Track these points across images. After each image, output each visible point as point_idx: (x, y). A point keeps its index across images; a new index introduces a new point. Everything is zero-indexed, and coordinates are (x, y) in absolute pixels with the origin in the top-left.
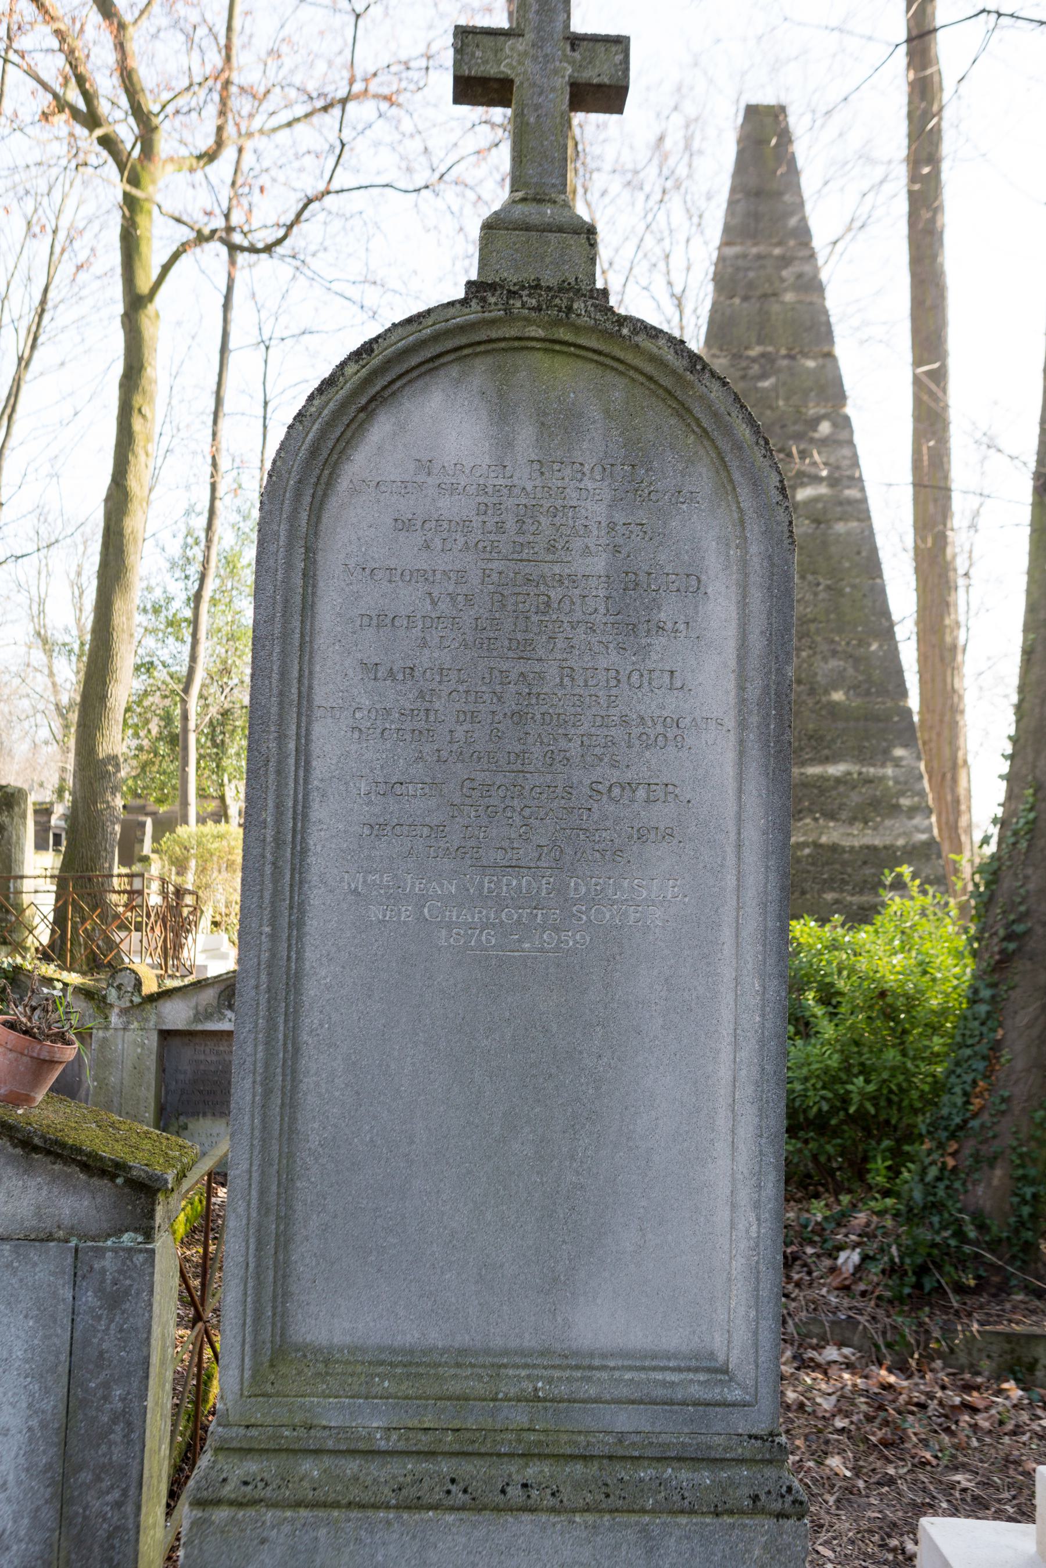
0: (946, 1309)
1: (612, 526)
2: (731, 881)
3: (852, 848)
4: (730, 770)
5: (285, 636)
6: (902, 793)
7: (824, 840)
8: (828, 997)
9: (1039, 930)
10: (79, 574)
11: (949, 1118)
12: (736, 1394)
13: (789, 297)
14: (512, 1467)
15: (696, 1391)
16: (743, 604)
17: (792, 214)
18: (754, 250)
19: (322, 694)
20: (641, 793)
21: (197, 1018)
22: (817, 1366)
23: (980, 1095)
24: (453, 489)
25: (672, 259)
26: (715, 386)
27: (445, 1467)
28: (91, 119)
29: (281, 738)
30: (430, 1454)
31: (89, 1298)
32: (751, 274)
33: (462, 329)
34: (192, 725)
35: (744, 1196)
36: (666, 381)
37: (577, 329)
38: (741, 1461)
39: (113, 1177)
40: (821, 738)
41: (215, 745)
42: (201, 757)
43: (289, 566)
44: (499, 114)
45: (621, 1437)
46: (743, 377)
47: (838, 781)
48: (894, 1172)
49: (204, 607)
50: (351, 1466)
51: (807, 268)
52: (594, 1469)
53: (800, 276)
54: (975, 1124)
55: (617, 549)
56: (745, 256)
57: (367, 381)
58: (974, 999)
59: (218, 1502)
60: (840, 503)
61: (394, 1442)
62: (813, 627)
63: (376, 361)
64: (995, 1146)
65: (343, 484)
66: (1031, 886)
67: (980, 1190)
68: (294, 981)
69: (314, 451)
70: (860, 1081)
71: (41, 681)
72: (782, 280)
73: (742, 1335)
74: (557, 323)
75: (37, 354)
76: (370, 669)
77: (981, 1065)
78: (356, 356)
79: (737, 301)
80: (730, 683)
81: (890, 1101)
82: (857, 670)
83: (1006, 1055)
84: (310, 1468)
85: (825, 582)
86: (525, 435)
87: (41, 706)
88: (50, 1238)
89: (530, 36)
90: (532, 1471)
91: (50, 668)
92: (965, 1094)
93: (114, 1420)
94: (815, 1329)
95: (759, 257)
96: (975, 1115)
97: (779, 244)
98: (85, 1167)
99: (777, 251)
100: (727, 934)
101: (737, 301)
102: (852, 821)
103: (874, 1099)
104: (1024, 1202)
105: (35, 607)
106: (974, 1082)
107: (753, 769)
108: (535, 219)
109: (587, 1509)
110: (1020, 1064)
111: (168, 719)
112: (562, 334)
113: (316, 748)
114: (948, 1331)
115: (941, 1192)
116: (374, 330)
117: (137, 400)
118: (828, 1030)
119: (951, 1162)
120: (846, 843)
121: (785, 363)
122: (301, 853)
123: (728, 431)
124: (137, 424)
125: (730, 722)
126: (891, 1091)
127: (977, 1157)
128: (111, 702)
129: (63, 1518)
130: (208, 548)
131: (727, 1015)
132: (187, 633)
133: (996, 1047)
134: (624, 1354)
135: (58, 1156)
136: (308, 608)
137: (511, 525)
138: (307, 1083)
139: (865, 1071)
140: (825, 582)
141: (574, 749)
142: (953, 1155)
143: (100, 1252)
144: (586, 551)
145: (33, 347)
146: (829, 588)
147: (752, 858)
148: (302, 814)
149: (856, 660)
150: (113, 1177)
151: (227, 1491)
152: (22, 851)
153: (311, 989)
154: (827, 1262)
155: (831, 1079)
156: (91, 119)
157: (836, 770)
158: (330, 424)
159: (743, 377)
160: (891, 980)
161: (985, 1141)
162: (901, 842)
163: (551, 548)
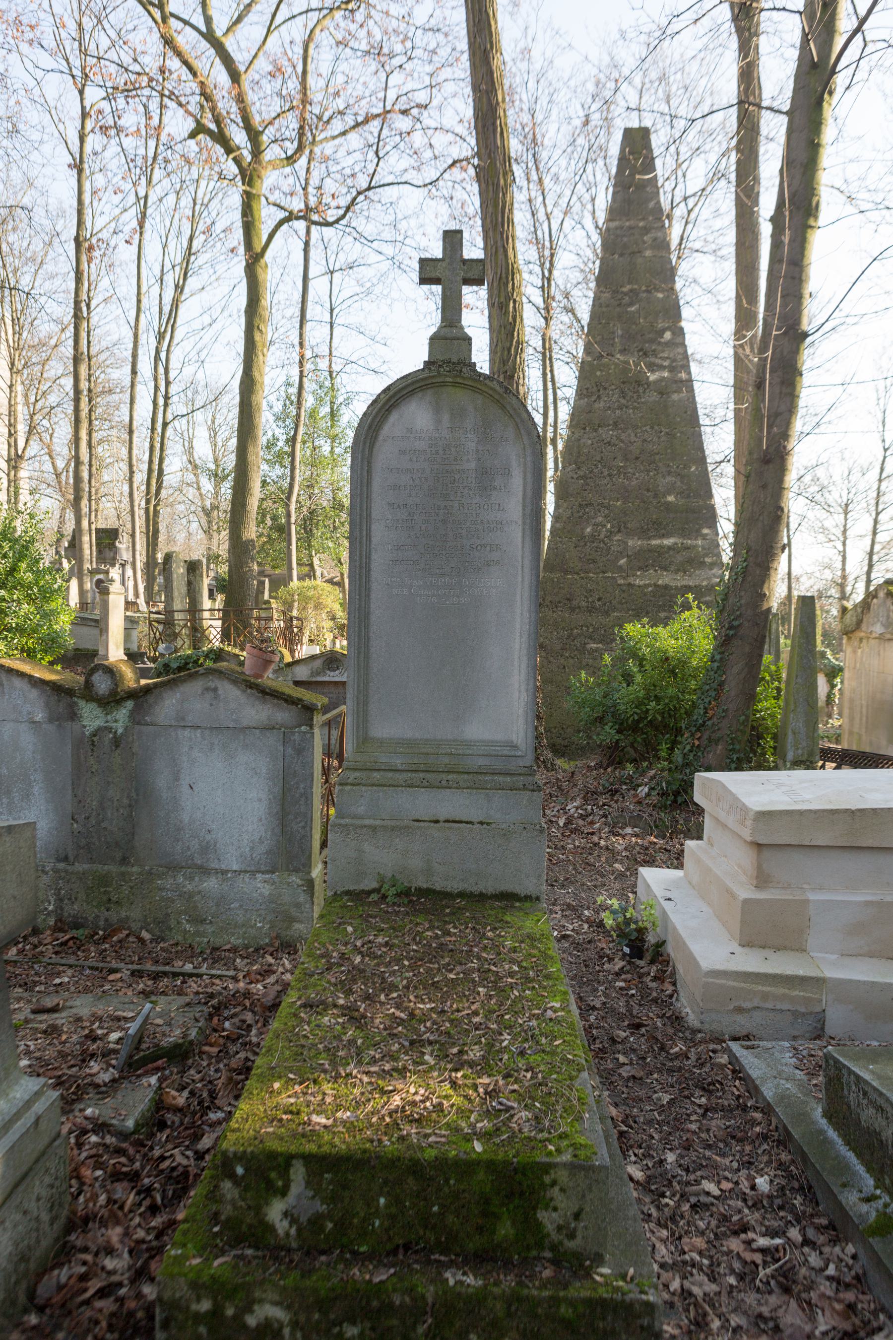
0: (688, 812)
1: (477, 451)
2: (520, 579)
3: (676, 587)
4: (520, 540)
5: (361, 494)
6: (707, 555)
7: (660, 582)
8: (641, 662)
9: (746, 624)
10: (213, 422)
11: (697, 720)
12: (520, 753)
13: (648, 253)
14: (444, 776)
15: (505, 752)
16: (525, 479)
17: (651, 199)
18: (627, 224)
19: (375, 513)
20: (488, 548)
21: (312, 675)
22: (619, 835)
23: (712, 709)
24: (420, 439)
25: (597, 202)
26: (514, 398)
27: (421, 775)
28: (221, 138)
29: (361, 530)
30: (416, 771)
31: (290, 750)
32: (625, 239)
33: (422, 380)
34: (293, 520)
35: (523, 687)
36: (496, 397)
37: (464, 378)
38: (520, 774)
39: (297, 705)
40: (661, 523)
41: (306, 532)
42: (298, 539)
43: (362, 469)
44: (438, 289)
45: (480, 767)
46: (619, 305)
47: (669, 548)
48: (672, 749)
49: (298, 446)
50: (390, 774)
51: (659, 234)
52: (471, 776)
53: (655, 239)
54: (709, 723)
55: (479, 459)
56: (622, 228)
57: (388, 400)
58: (712, 660)
59: (347, 784)
60: (676, 382)
61: (404, 767)
62: (657, 457)
63: (391, 393)
64: (719, 734)
65: (381, 438)
66: (743, 602)
67: (710, 756)
68: (367, 615)
69: (370, 427)
70: (653, 704)
71: (191, 492)
72: (644, 243)
73: (522, 734)
74: (457, 376)
75: (187, 283)
76: (391, 505)
77: (713, 694)
78: (384, 391)
79: (616, 256)
80: (520, 508)
81: (670, 716)
82: (682, 482)
83: (726, 688)
84: (377, 775)
85: (665, 430)
86: (446, 417)
87: (193, 508)
88: (273, 728)
89: (447, 261)
90: (450, 777)
91: (198, 484)
92: (705, 708)
93: (301, 796)
94: (621, 820)
95: (630, 228)
96: (710, 719)
97: (643, 219)
98: (286, 701)
99: (641, 224)
100: (518, 597)
101: (616, 256)
102: (677, 571)
103: (662, 714)
104: (732, 761)
105: (186, 444)
106: (710, 702)
107: (528, 539)
108: (449, 335)
109: (468, 788)
110: (733, 693)
111: (274, 518)
112: (458, 380)
113: (373, 534)
114: (687, 820)
115: (691, 758)
116: (390, 382)
117: (257, 321)
118: (638, 678)
119: (697, 743)
120: (673, 584)
121: (644, 295)
122: (369, 571)
123: (519, 415)
124: (257, 337)
125: (520, 522)
126: (670, 709)
127: (710, 740)
128: (249, 508)
129: (283, 832)
130: (299, 408)
131: (518, 626)
132: (287, 462)
133: (721, 684)
134: (483, 741)
135: (276, 696)
136: (369, 484)
137: (441, 452)
138: (373, 650)
139: (657, 698)
140: (665, 430)
141: (464, 532)
142: (698, 739)
143: (293, 733)
144: (468, 461)
145: (185, 279)
146: (667, 434)
147: (527, 570)
148: (369, 557)
149: (682, 477)
150: (297, 705)
151: (349, 781)
152: (202, 596)
153: (373, 618)
154: (632, 792)
155: (640, 704)
156: (221, 138)
157: (668, 542)
158: (375, 417)
159: (619, 305)
160: (671, 653)
161: (714, 732)
162: (705, 583)
163: (456, 459)
